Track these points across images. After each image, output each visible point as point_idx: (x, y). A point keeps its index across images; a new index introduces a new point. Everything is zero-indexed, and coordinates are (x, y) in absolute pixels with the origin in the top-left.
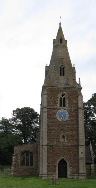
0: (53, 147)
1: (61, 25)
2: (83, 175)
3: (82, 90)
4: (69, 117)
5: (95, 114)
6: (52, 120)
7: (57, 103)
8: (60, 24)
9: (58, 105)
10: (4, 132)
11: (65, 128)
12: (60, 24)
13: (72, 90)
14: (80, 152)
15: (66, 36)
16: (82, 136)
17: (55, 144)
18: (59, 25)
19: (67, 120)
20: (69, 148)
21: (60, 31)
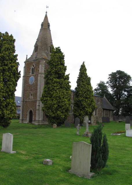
0: (27, 102)
1: (47, 14)
2: (37, 121)
3: (32, 55)
4: (35, 81)
5: (58, 76)
6: (27, 84)
7: (30, 72)
8: (46, 12)
9: (31, 73)
10: (101, 92)
11: (33, 89)
12: (46, 12)
13: (38, 61)
14: (37, 105)
15: (50, 21)
16: (39, 93)
17: (28, 100)
18: (45, 13)
19: (34, 83)
20: (34, 103)
21: (46, 17)
